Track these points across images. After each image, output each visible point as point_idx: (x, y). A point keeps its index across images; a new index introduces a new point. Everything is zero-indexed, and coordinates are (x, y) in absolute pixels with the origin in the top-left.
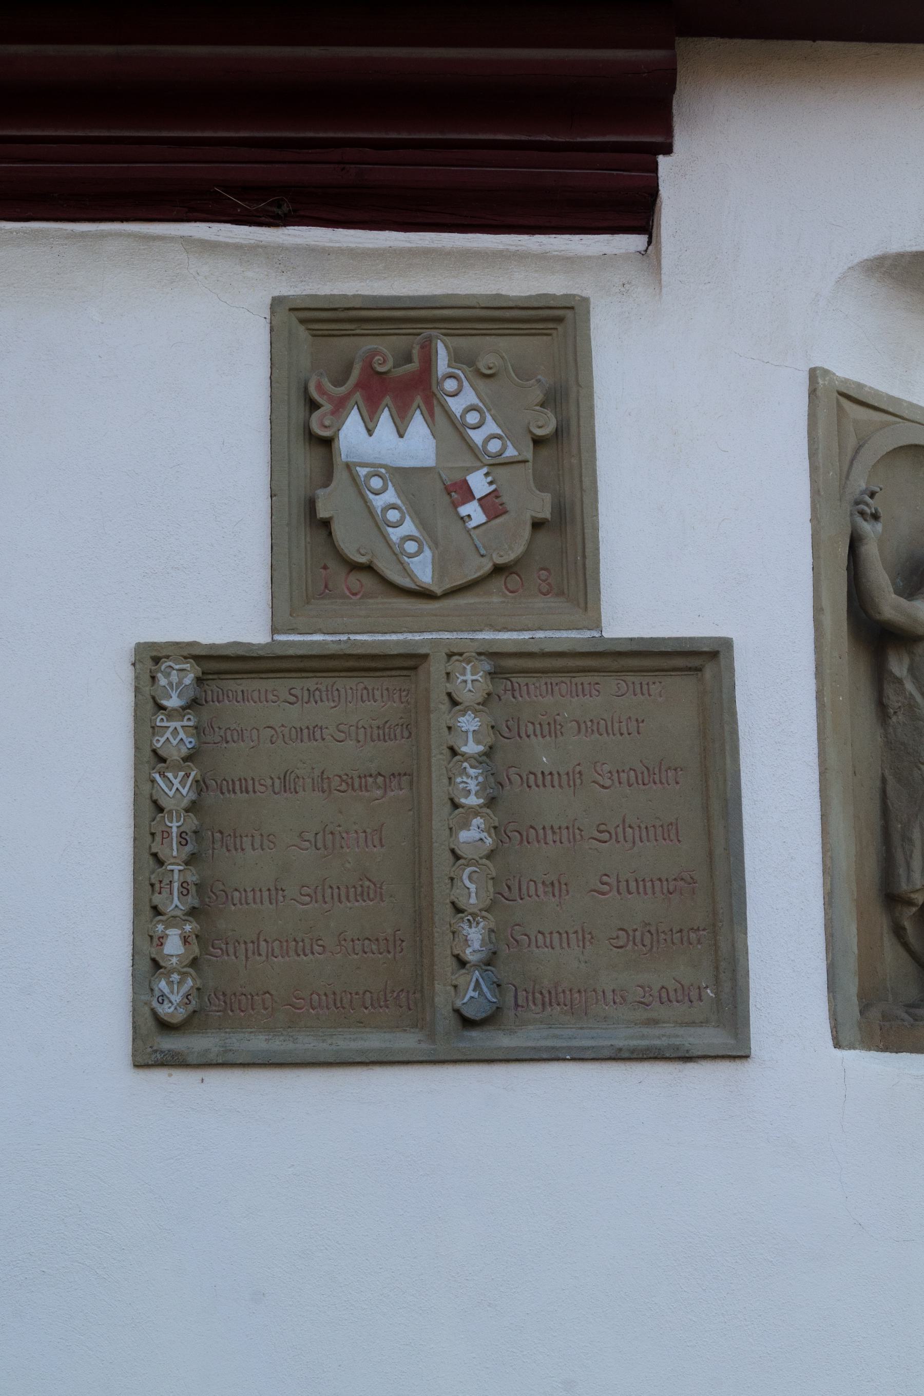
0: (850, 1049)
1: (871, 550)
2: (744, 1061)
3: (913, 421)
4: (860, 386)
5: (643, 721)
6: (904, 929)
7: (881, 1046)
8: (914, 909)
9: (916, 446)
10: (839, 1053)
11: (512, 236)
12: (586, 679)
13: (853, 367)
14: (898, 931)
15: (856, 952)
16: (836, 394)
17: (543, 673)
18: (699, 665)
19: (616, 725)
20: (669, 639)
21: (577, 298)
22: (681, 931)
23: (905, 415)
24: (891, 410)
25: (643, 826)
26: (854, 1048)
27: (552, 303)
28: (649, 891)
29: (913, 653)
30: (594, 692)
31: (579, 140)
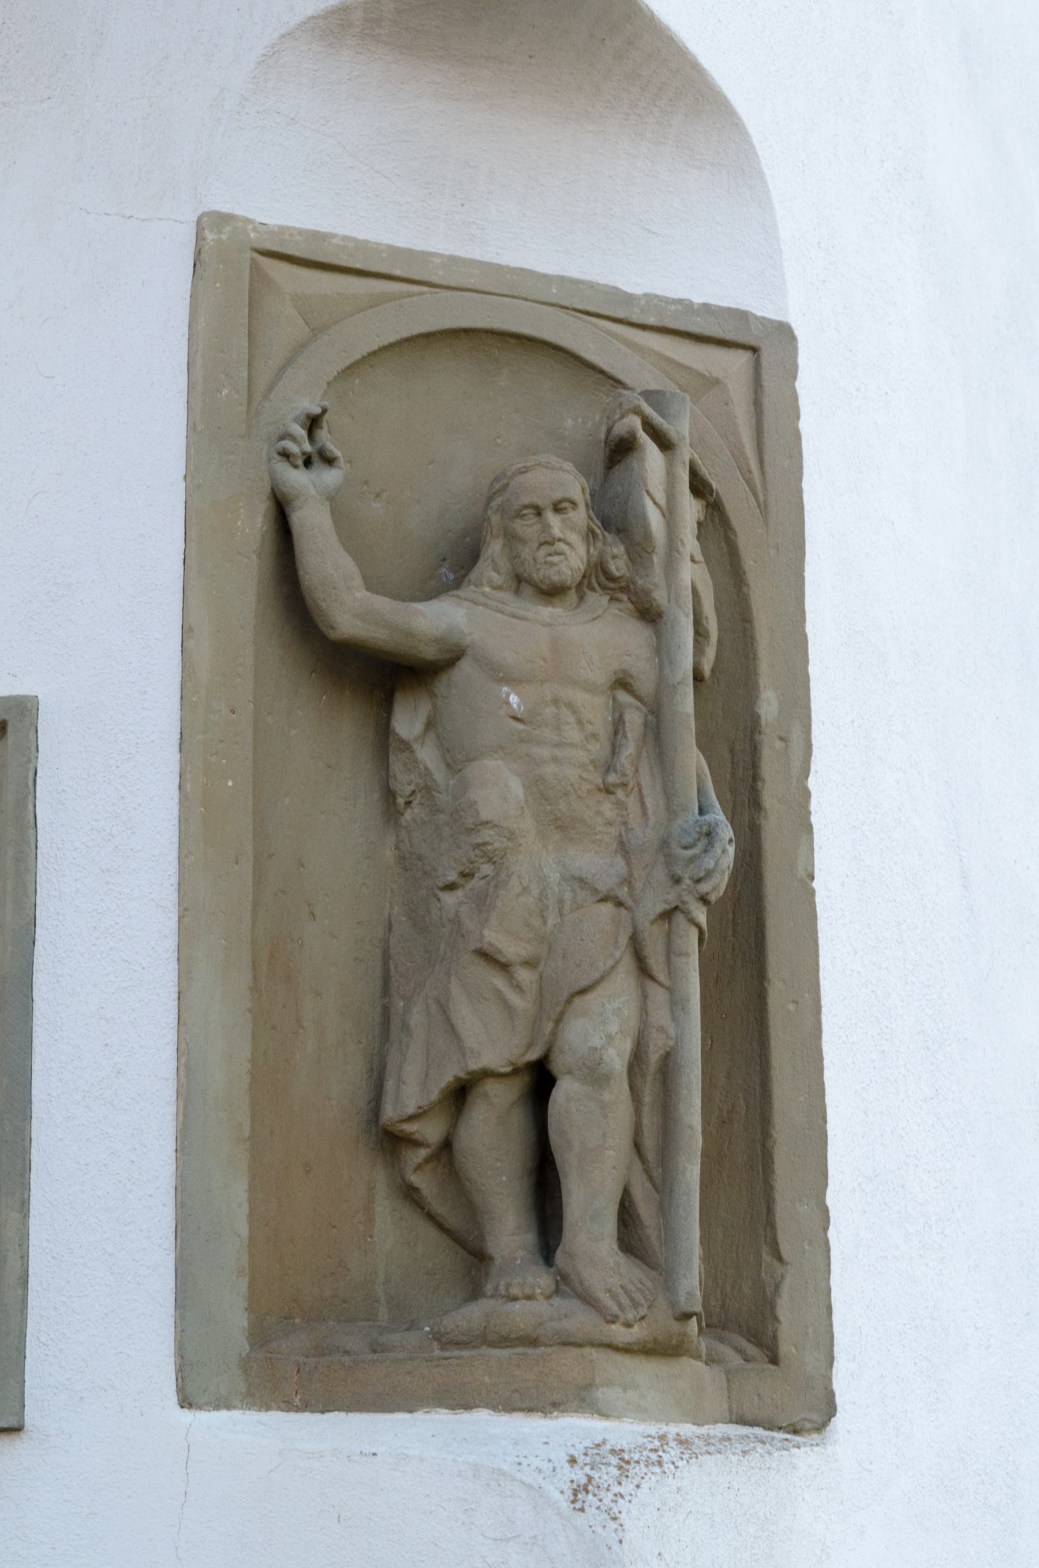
0: (217, 1408)
1: (312, 521)
2: (13, 1436)
3: (490, 294)
6: (416, 1190)
7: (297, 1401)
8: (423, 1153)
9: (467, 331)
14: (410, 1194)
15: (244, 1230)
16: (249, 254)
23: (435, 279)
24: (397, 272)
26: (229, 1407)
29: (436, 695)
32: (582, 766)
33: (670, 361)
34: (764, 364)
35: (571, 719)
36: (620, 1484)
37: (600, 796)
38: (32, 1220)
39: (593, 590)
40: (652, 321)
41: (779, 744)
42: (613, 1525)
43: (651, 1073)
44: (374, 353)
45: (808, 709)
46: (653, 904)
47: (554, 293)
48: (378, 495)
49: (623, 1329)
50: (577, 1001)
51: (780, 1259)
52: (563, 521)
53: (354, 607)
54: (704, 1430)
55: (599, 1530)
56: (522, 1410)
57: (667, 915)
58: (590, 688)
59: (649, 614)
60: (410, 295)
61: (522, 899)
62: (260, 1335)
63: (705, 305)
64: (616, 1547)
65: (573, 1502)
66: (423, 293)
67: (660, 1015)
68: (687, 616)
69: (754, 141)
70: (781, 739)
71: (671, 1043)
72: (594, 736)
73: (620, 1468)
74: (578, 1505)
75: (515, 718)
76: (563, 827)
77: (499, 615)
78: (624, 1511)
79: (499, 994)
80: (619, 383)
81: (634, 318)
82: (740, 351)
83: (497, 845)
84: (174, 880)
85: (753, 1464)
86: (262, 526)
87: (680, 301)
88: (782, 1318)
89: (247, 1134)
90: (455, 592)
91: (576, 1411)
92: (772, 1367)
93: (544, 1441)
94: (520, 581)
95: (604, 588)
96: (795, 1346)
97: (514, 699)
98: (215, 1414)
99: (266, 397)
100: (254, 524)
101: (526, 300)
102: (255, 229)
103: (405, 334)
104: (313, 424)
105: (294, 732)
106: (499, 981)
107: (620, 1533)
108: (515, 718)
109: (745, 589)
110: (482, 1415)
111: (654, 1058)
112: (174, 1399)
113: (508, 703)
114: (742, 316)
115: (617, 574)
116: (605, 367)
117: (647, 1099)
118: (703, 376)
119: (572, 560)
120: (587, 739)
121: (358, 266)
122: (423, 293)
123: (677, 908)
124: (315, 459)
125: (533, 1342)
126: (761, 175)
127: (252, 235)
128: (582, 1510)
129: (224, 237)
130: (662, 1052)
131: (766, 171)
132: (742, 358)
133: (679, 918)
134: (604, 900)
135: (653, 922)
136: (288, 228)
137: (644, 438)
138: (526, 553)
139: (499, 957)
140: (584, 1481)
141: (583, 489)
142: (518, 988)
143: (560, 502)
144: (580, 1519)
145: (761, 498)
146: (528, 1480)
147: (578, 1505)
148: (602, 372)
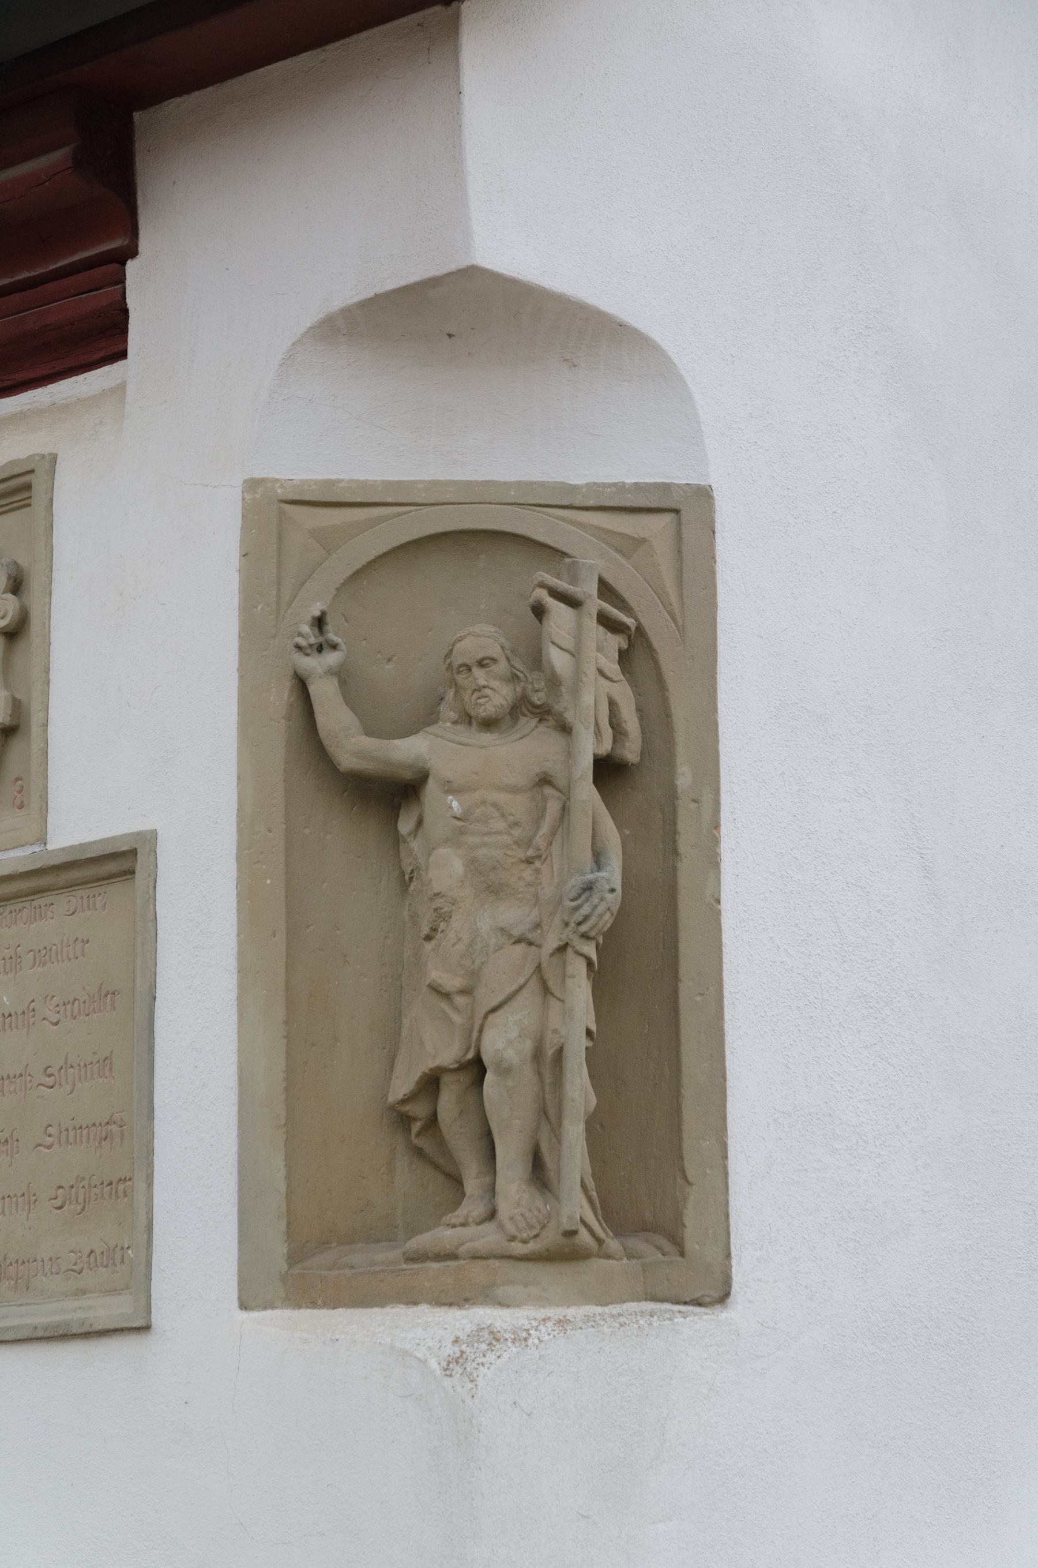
0: (265, 1308)
1: (325, 693)
3: (459, 504)
4: (330, 483)
5: (88, 941)
6: (421, 1149)
7: (320, 1302)
10: (244, 1315)
11: (30, 392)
12: (41, 901)
13: (309, 460)
17: (34, 894)
18: (117, 866)
19: (65, 949)
20: (95, 842)
21: (37, 458)
22: (111, 1184)
24: (390, 500)
25: (82, 1064)
26: (273, 1308)
27: (18, 470)
28: (84, 1139)
30: (50, 914)
31: (52, 267)
32: (508, 846)
33: (606, 531)
34: (684, 520)
35: (496, 814)
36: (484, 1356)
37: (523, 866)
38: (155, 1188)
39: (525, 715)
40: (591, 503)
41: (693, 806)
42: (470, 1385)
43: (548, 1062)
44: (373, 561)
45: (717, 776)
46: (552, 942)
47: (512, 495)
48: (389, 660)
49: (520, 1245)
50: (491, 1017)
51: (687, 1181)
52: (487, 673)
53: (353, 746)
54: (607, 1310)
55: (459, 1389)
56: (445, 1304)
57: (562, 949)
58: (514, 790)
59: (565, 729)
60: (381, 520)
61: (457, 947)
62: (294, 1258)
63: (636, 484)
64: (469, 1400)
65: (445, 1370)
66: (410, 512)
67: (554, 1020)
68: (587, 728)
69: (670, 353)
70: (694, 801)
71: (562, 1040)
72: (516, 824)
73: (490, 1344)
74: (448, 1373)
75: (456, 818)
76: (493, 890)
77: (450, 744)
78: (481, 1375)
79: (444, 1012)
80: (564, 554)
81: (578, 503)
82: (667, 514)
83: (446, 909)
84: (235, 951)
85: (629, 1333)
86: (289, 698)
87: (615, 485)
88: (687, 1224)
89: (283, 1122)
90: (429, 729)
91: (482, 1304)
92: (681, 1259)
93: (428, 1330)
94: (467, 719)
95: (533, 713)
96: (697, 1243)
97: (455, 804)
98: (264, 1313)
99: (289, 605)
100: (280, 697)
101: (490, 503)
102: (282, 486)
103: (395, 544)
104: (320, 623)
105: (329, 836)
106: (444, 1006)
107: (474, 1391)
108: (456, 818)
109: (667, 694)
110: (424, 1308)
111: (550, 1052)
112: (236, 1304)
113: (451, 807)
114: (665, 488)
115: (539, 703)
116: (552, 544)
117: (548, 1081)
118: (634, 538)
119: (498, 697)
120: (510, 827)
121: (359, 500)
122: (410, 512)
123: (567, 944)
124: (325, 646)
125: (453, 1256)
126: (681, 378)
127: (279, 491)
128: (451, 1376)
129: (258, 496)
130: (557, 1047)
131: (683, 373)
132: (668, 518)
133: (569, 950)
134: (518, 941)
135: (552, 955)
136: (307, 480)
137: (550, 602)
138: (466, 697)
139: (440, 989)
140: (458, 1354)
141: (502, 648)
142: (456, 1009)
143: (483, 659)
144: (447, 1382)
145: (680, 623)
146: (420, 1356)
147: (448, 1373)
148: (550, 547)
